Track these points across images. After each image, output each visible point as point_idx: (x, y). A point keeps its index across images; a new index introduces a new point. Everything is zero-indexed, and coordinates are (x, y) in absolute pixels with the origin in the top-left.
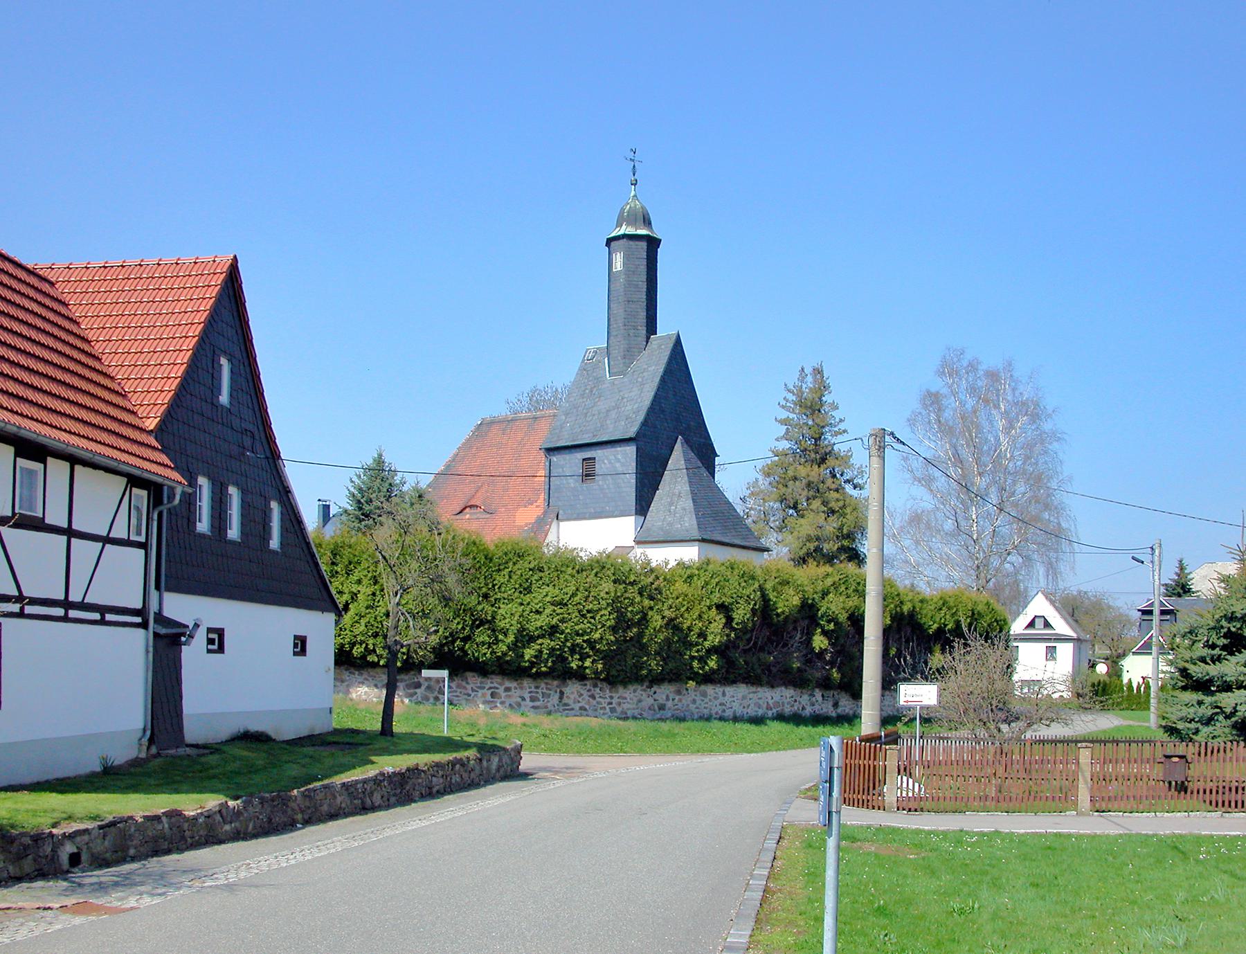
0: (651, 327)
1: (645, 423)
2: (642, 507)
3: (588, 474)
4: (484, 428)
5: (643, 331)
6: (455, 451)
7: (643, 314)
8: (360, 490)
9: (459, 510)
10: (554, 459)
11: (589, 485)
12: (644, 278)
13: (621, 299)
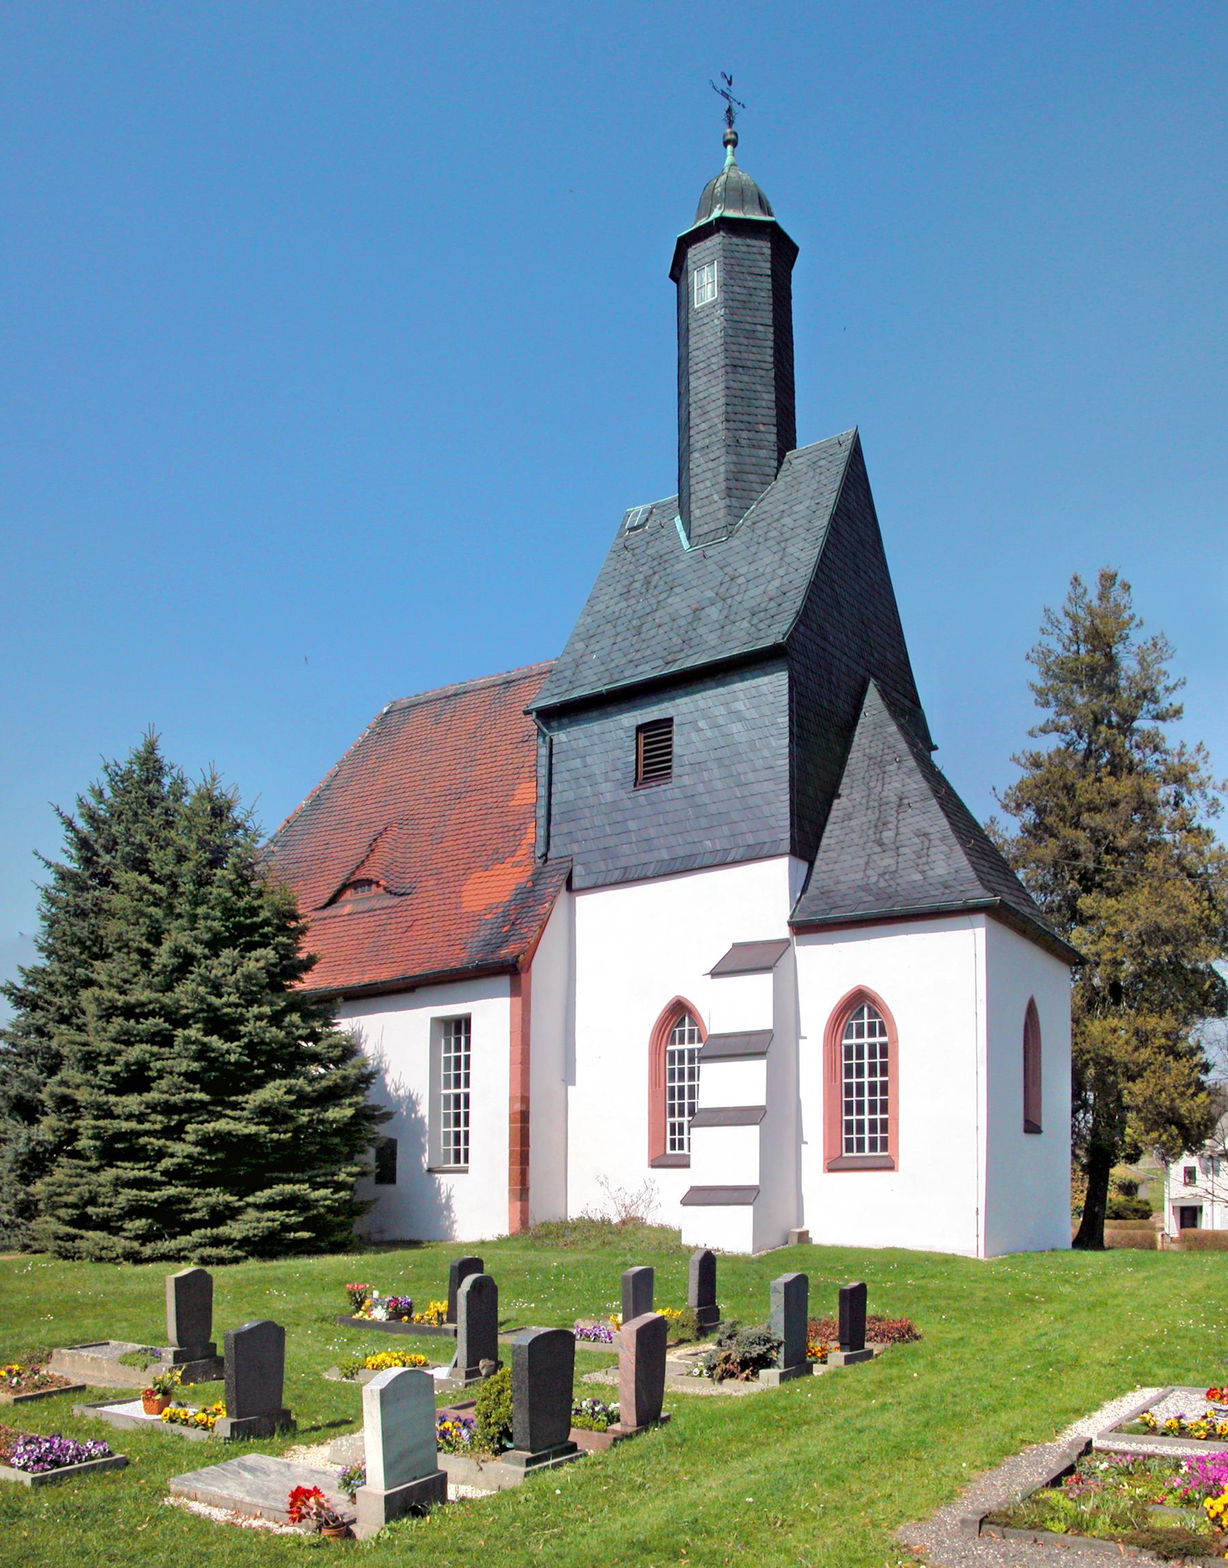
0: (786, 439)
1: (803, 618)
2: (805, 843)
3: (655, 754)
4: (395, 718)
5: (770, 436)
6: (332, 767)
7: (768, 397)
8: (92, 818)
9: (327, 896)
10: (561, 737)
11: (659, 791)
12: (768, 318)
13: (718, 361)
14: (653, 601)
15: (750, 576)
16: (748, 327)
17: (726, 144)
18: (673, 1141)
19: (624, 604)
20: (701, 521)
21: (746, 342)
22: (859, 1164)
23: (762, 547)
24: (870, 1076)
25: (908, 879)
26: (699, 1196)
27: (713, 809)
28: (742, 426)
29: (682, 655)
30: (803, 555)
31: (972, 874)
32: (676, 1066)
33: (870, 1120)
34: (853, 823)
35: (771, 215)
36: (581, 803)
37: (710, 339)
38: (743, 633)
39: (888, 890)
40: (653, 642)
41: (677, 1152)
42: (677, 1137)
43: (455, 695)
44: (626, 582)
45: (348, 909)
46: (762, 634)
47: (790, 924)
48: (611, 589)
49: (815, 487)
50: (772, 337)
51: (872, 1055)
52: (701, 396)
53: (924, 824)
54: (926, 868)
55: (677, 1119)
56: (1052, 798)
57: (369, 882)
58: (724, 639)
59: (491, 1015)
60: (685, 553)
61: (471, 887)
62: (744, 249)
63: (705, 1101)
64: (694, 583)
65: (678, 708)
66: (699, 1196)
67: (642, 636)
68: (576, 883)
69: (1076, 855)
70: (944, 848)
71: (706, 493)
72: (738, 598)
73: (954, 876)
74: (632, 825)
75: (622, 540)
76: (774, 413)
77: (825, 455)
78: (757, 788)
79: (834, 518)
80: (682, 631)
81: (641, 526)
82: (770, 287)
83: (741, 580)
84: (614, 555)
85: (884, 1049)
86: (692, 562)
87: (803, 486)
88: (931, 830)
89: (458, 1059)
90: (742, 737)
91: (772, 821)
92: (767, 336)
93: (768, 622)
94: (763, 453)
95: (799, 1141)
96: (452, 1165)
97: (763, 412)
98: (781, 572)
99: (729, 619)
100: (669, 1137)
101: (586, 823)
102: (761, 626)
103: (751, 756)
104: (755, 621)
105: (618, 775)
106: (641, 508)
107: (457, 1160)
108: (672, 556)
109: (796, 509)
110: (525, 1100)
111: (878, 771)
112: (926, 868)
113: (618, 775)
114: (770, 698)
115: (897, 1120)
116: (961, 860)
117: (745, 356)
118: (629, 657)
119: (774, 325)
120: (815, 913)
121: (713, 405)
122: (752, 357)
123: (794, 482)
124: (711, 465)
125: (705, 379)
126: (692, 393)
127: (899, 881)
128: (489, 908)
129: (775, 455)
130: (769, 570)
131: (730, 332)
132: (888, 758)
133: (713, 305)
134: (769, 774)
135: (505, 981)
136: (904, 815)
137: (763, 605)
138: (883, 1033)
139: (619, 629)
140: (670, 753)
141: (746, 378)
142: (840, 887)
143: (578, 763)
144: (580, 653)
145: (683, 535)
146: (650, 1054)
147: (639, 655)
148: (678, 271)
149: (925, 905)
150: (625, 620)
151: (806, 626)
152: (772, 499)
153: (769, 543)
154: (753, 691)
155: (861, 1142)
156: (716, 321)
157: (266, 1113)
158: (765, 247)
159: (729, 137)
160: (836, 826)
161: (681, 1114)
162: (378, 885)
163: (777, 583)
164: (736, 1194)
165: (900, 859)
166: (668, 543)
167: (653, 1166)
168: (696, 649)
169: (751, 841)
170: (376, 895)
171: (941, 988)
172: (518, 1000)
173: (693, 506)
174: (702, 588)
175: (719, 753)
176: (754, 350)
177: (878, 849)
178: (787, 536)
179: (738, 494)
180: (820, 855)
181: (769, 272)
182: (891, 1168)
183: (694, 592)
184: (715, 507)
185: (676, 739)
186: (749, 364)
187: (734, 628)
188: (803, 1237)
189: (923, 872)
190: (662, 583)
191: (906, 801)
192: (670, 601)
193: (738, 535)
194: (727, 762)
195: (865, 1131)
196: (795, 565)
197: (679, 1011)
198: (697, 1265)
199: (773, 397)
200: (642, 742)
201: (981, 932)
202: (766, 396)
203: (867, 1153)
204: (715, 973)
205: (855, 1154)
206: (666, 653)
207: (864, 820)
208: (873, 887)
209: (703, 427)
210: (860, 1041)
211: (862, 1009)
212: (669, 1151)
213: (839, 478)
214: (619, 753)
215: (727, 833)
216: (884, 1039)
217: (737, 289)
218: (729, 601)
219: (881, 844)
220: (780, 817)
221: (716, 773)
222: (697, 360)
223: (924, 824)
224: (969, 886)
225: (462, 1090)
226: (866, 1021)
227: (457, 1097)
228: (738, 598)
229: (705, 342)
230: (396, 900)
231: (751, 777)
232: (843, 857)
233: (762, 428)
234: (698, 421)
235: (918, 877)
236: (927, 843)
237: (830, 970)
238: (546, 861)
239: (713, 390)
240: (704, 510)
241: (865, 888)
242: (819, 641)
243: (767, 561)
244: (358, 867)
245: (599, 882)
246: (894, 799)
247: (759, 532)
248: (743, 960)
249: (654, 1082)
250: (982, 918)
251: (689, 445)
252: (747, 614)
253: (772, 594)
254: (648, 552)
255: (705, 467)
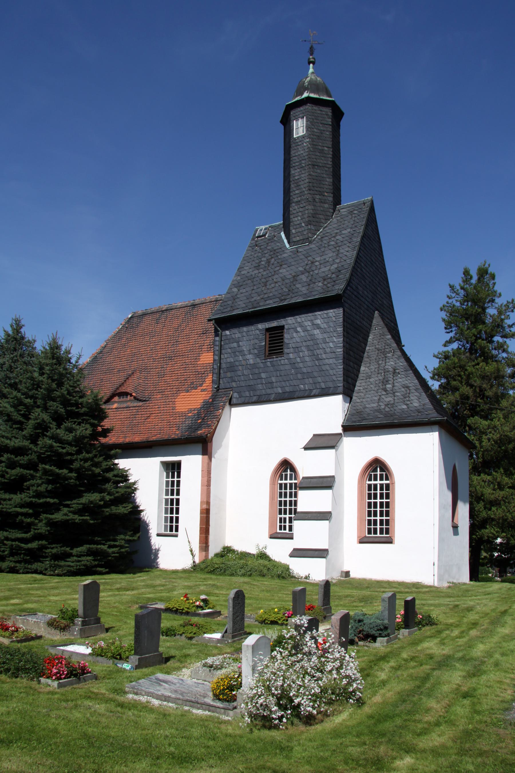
0: (337, 200)
1: (349, 283)
3: (275, 343)
12: (330, 144)
14: (272, 271)
15: (322, 262)
16: (320, 148)
17: (309, 63)
18: (280, 526)
19: (256, 272)
20: (296, 235)
21: (319, 154)
22: (376, 540)
23: (326, 249)
24: (380, 499)
25: (399, 407)
26: (298, 553)
27: (305, 370)
28: (316, 192)
29: (289, 297)
30: (348, 254)
31: (431, 407)
32: (283, 491)
33: (380, 520)
34: (371, 380)
35: (331, 97)
36: (237, 363)
37: (302, 152)
38: (319, 288)
39: (391, 412)
40: (274, 290)
41: (283, 531)
42: (283, 524)
43: (166, 310)
44: (257, 261)
45: (115, 406)
46: (330, 289)
47: (342, 426)
48: (249, 264)
49: (352, 223)
50: (331, 153)
51: (382, 489)
52: (296, 178)
53: (407, 382)
54: (409, 403)
55: (283, 516)
56: (450, 369)
57: (126, 394)
58: (310, 290)
59: (191, 464)
60: (287, 249)
61: (180, 400)
62: (319, 112)
63: (300, 508)
64: (293, 263)
65: (289, 322)
66: (298, 553)
67: (268, 287)
68: (234, 401)
69: (468, 398)
70: (417, 394)
71: (298, 222)
72: (316, 272)
73: (422, 407)
74: (263, 375)
75: (254, 242)
76: (331, 187)
77: (356, 209)
78: (327, 361)
79: (363, 237)
80: (288, 285)
81: (264, 235)
82: (331, 130)
83: (317, 263)
84: (250, 248)
85: (388, 487)
86: (291, 254)
87: (346, 222)
88: (410, 385)
89: (173, 482)
90: (320, 336)
91: (334, 378)
92: (329, 152)
93: (333, 283)
94: (326, 206)
95: (176, 456)
96: (169, 532)
97: (326, 187)
98: (337, 261)
99: (311, 282)
100: (278, 524)
101: (239, 373)
102: (329, 285)
103: (324, 345)
104: (325, 283)
105: (256, 351)
106: (263, 227)
107: (171, 530)
108: (280, 250)
109: (343, 232)
110: (208, 503)
111: (383, 356)
112: (409, 403)
113: (256, 351)
114: (334, 319)
115: (394, 520)
116: (427, 401)
117: (318, 161)
118: (261, 296)
119: (333, 148)
120: (355, 422)
121: (302, 182)
122: (322, 161)
123: (341, 220)
124: (301, 210)
125: (298, 170)
126: (291, 176)
127: (396, 408)
128: (190, 411)
129: (332, 207)
130: (331, 260)
131: (311, 149)
132: (387, 350)
133: (303, 137)
134: (333, 355)
135: (200, 447)
136: (397, 377)
137: (329, 276)
138: (387, 479)
139: (255, 283)
140: (282, 342)
141: (319, 171)
142: (366, 410)
143: (235, 345)
144: (235, 293)
145: (285, 241)
146: (270, 484)
147: (266, 296)
148: (286, 121)
149: (409, 420)
150: (257, 279)
151: (351, 287)
152: (330, 227)
153: (331, 247)
154: (325, 316)
155: (375, 530)
156: (305, 144)
157: (84, 510)
158: (328, 111)
159: (312, 60)
160: (363, 381)
161: (285, 513)
162: (131, 395)
163: (335, 266)
164: (317, 553)
165: (396, 398)
166: (278, 244)
167: (271, 538)
168: (296, 295)
169: (324, 387)
170: (130, 400)
171: (418, 460)
172: (206, 457)
173: (291, 228)
174: (298, 266)
175: (308, 343)
176: (323, 158)
177: (384, 393)
178: (340, 244)
179: (314, 223)
180: (355, 394)
181: (331, 123)
182: (391, 542)
183: (293, 267)
184: (303, 229)
185: (286, 336)
186: (320, 165)
187: (315, 286)
188: (347, 574)
189: (407, 405)
190: (276, 262)
191: (397, 371)
192: (281, 271)
193: (314, 242)
194: (312, 349)
195: (378, 525)
196: (345, 258)
197: (286, 466)
198: (342, 615)
199: (331, 180)
200: (268, 336)
201: (436, 435)
202: (328, 180)
203: (378, 535)
204: (306, 448)
205: (372, 535)
206: (280, 295)
207: (377, 379)
208: (383, 411)
209: (297, 192)
210: (375, 482)
211: (377, 468)
212: (278, 531)
213: (365, 219)
214: (256, 341)
215: (311, 382)
216: (388, 482)
217: (315, 130)
218: (311, 273)
219: (385, 390)
220: (338, 376)
221: (306, 353)
222: (294, 161)
223: (407, 382)
224: (430, 412)
225: (175, 497)
226: (378, 473)
227: (172, 500)
228: (316, 272)
229: (299, 153)
230: (141, 404)
231: (324, 356)
232: (367, 396)
233: (326, 194)
234: (295, 189)
235: (405, 407)
236: (408, 391)
237: (360, 449)
238: (218, 390)
239: (303, 176)
240: (298, 230)
241: (379, 411)
242: (355, 293)
243: (330, 255)
244: (120, 386)
245: (246, 401)
246: (391, 370)
247: (325, 242)
248: (321, 442)
249: (272, 498)
250: (436, 427)
251: (289, 200)
252: (321, 279)
253: (333, 271)
254: (268, 248)
255: (298, 210)
